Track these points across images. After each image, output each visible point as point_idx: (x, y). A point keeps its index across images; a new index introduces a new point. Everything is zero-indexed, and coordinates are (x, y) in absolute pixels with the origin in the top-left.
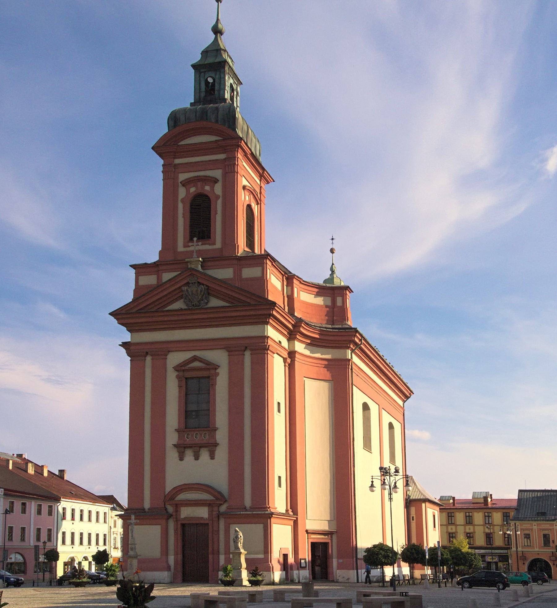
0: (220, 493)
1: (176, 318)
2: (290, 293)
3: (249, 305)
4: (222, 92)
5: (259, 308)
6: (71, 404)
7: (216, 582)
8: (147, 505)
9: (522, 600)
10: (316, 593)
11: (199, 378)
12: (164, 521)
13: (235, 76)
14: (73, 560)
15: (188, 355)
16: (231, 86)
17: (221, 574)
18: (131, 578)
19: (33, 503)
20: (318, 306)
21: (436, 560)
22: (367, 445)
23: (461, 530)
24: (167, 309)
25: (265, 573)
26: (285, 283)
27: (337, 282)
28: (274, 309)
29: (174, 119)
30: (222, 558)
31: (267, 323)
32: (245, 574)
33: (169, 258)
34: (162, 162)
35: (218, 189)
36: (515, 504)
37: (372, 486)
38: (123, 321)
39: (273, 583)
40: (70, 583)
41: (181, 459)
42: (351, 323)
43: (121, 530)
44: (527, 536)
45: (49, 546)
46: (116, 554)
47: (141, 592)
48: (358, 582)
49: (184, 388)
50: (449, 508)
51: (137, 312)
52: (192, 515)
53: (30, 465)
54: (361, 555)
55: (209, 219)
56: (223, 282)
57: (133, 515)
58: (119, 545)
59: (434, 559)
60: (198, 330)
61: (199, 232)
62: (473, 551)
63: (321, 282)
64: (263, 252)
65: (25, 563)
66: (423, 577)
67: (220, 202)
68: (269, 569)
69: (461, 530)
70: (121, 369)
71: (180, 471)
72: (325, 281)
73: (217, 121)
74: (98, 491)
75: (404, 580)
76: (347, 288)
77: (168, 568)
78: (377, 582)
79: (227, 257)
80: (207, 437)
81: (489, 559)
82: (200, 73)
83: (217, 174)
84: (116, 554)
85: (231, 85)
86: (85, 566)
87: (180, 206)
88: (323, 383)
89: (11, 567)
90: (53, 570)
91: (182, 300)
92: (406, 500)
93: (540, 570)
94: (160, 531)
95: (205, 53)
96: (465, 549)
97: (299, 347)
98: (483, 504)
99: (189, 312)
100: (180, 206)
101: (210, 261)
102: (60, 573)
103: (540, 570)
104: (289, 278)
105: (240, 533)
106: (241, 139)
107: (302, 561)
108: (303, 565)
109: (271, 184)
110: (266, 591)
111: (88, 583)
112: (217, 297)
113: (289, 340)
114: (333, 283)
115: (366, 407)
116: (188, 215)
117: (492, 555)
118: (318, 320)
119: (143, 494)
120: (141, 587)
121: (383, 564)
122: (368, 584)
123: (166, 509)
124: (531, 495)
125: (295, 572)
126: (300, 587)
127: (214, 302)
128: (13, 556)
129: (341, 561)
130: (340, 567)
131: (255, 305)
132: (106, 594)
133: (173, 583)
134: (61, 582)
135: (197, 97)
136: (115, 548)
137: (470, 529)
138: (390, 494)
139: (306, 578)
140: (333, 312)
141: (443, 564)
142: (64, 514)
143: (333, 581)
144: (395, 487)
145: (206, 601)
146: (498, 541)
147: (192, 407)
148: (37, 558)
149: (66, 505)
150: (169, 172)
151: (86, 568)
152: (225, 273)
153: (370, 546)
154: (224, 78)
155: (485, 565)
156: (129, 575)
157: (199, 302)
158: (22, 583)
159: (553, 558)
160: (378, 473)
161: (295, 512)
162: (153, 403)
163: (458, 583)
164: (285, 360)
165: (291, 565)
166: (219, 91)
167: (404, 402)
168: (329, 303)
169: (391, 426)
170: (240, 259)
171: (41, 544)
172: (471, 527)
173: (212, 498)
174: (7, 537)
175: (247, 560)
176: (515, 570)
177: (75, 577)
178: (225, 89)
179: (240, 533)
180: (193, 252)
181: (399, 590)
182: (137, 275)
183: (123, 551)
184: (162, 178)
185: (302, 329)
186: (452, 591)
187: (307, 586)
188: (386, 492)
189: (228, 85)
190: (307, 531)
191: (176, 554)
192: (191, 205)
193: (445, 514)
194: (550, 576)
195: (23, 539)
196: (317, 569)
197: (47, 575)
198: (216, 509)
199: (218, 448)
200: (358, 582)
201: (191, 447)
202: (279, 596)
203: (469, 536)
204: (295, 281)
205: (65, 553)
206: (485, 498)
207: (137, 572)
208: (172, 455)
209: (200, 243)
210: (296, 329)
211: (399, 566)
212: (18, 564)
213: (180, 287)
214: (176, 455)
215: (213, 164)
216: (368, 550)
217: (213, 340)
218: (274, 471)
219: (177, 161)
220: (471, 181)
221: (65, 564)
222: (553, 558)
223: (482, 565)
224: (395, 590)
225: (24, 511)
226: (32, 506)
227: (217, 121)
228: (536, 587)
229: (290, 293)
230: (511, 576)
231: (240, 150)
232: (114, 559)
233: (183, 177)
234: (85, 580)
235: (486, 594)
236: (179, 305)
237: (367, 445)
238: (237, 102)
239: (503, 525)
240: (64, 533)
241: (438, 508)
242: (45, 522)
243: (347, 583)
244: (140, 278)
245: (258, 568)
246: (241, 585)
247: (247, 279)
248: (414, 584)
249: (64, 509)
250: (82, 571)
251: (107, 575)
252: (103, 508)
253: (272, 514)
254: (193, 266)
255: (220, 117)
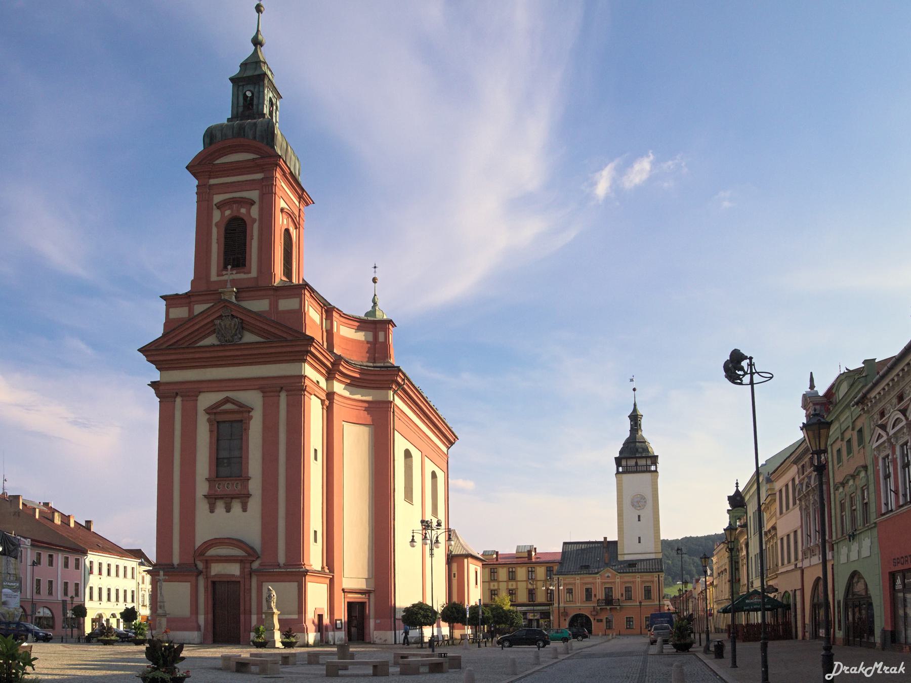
0: (252, 548)
1: (208, 355)
2: (329, 328)
3: (286, 340)
4: (260, 107)
5: (297, 345)
6: (94, 449)
7: (248, 644)
8: (176, 561)
9: (561, 657)
10: (352, 656)
11: (232, 422)
12: (194, 578)
13: (275, 90)
14: (100, 616)
15: (220, 396)
16: (271, 100)
17: (253, 635)
18: (160, 637)
19: (60, 555)
20: (359, 341)
21: (477, 618)
22: (409, 496)
23: (503, 586)
24: (198, 345)
25: (299, 635)
26: (324, 316)
27: (379, 316)
28: (311, 345)
29: (211, 136)
30: (254, 618)
31: (305, 361)
32: (278, 636)
33: (202, 288)
34: (196, 182)
35: (255, 212)
36: (559, 558)
37: (413, 541)
38: (152, 359)
39: (307, 645)
40: (99, 641)
41: (212, 511)
42: (394, 361)
43: (150, 587)
44: (570, 591)
45: (77, 601)
46: (144, 612)
47: (170, 652)
48: (395, 643)
49: (215, 433)
50: (492, 564)
51: (166, 349)
52: (223, 572)
53: (56, 514)
54: (399, 615)
55: (245, 244)
56: (258, 315)
57: (162, 571)
58: (147, 602)
59: (475, 617)
60: (231, 369)
61: (234, 259)
62: (514, 609)
63: (362, 315)
64: (301, 282)
65: (53, 618)
66: (463, 637)
67: (256, 226)
68: (303, 630)
69: (503, 586)
70: (149, 411)
71: (212, 523)
72: (366, 315)
73: (255, 138)
74: (125, 544)
75: (443, 640)
76: (390, 322)
77: (198, 628)
78: (416, 643)
79: (262, 287)
80: (239, 487)
81: (530, 616)
82: (239, 86)
83: (254, 195)
84: (144, 612)
85: (270, 99)
86: (113, 623)
87: (215, 231)
88: (362, 427)
89: (39, 621)
90: (81, 627)
91: (214, 335)
92: (448, 555)
93: (581, 625)
94: (189, 588)
95: (244, 65)
96: (507, 607)
97: (338, 387)
98: (527, 559)
99: (222, 348)
100: (215, 231)
101: (244, 291)
102: (88, 630)
103: (581, 625)
104: (328, 310)
105: (273, 591)
106: (280, 157)
107: (338, 622)
108: (339, 626)
109: (311, 206)
110: (300, 653)
111: (116, 641)
112: (252, 332)
113: (327, 380)
114: (375, 315)
115: (408, 454)
116: (222, 240)
117: (533, 611)
118: (358, 357)
119: (172, 548)
120: (171, 647)
121: (422, 625)
122: (406, 646)
123: (196, 565)
124: (575, 547)
125: (331, 634)
126: (335, 649)
127: (249, 338)
128: (41, 610)
129: (378, 621)
130: (378, 628)
131: (291, 341)
132: (135, 653)
133: (203, 644)
134: (89, 639)
135: (235, 112)
136: (143, 606)
137: (512, 585)
138: (432, 549)
139: (341, 640)
140: (375, 348)
141: (483, 623)
142: (91, 567)
143: (370, 643)
144: (437, 541)
145: (237, 663)
146: (541, 598)
147: (224, 454)
148: (65, 614)
149: (93, 558)
150: (204, 194)
151: (114, 626)
152: (260, 305)
153: (409, 605)
154: (263, 92)
155: (526, 623)
156: (158, 634)
157: (232, 337)
158: (51, 638)
159: (594, 613)
160: (419, 527)
161: (331, 570)
162: (183, 450)
163: (499, 643)
164: (323, 402)
165: (327, 626)
166: (258, 105)
167: (448, 448)
168: (371, 339)
169: (434, 475)
170: (277, 289)
171: (68, 599)
172: (514, 583)
173: (244, 554)
174: (35, 591)
175: (280, 620)
176: (556, 627)
177: (103, 634)
178: (263, 104)
179: (273, 591)
180: (226, 281)
181: (438, 651)
182: (168, 307)
183: (151, 609)
184: (196, 200)
185: (341, 368)
186: (493, 652)
187: (343, 648)
188: (428, 547)
189: (267, 98)
190: (343, 590)
191: (206, 613)
192: (226, 230)
193: (487, 570)
194: (590, 632)
195: (50, 593)
196: (353, 630)
197: (75, 631)
198: (248, 565)
199: (250, 499)
200: (395, 643)
201: (222, 498)
202: (313, 659)
203: (512, 593)
204: (334, 314)
205: (93, 608)
206: (529, 552)
207: (166, 632)
208: (202, 506)
209: (234, 272)
210: (336, 368)
211: (439, 626)
212: (46, 618)
213: (212, 321)
214: (207, 506)
215: (250, 185)
216: (407, 610)
217: (209, 381)
218: (309, 524)
219: (213, 181)
220: (520, 204)
221: (93, 621)
222: (594, 613)
223: (523, 622)
224: (433, 651)
225: (51, 564)
226: (59, 558)
227: (255, 138)
228: (575, 644)
229: (329, 328)
230: (552, 633)
231: (278, 169)
232: (143, 617)
233: (217, 199)
234: (113, 638)
235: (525, 653)
236: (211, 340)
237: (409, 496)
238: (277, 117)
239: (546, 580)
240: (91, 588)
241: (480, 564)
242: (71, 575)
243: (384, 644)
244: (297, 307)
245: (292, 629)
246: (274, 647)
247: (284, 312)
248: (453, 644)
249: (91, 562)
250: (110, 628)
251: (135, 633)
252: (131, 563)
253: (307, 571)
254: (226, 297)
255: (258, 133)
